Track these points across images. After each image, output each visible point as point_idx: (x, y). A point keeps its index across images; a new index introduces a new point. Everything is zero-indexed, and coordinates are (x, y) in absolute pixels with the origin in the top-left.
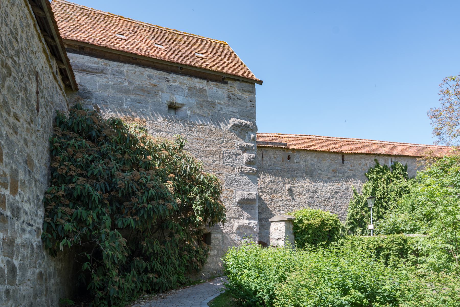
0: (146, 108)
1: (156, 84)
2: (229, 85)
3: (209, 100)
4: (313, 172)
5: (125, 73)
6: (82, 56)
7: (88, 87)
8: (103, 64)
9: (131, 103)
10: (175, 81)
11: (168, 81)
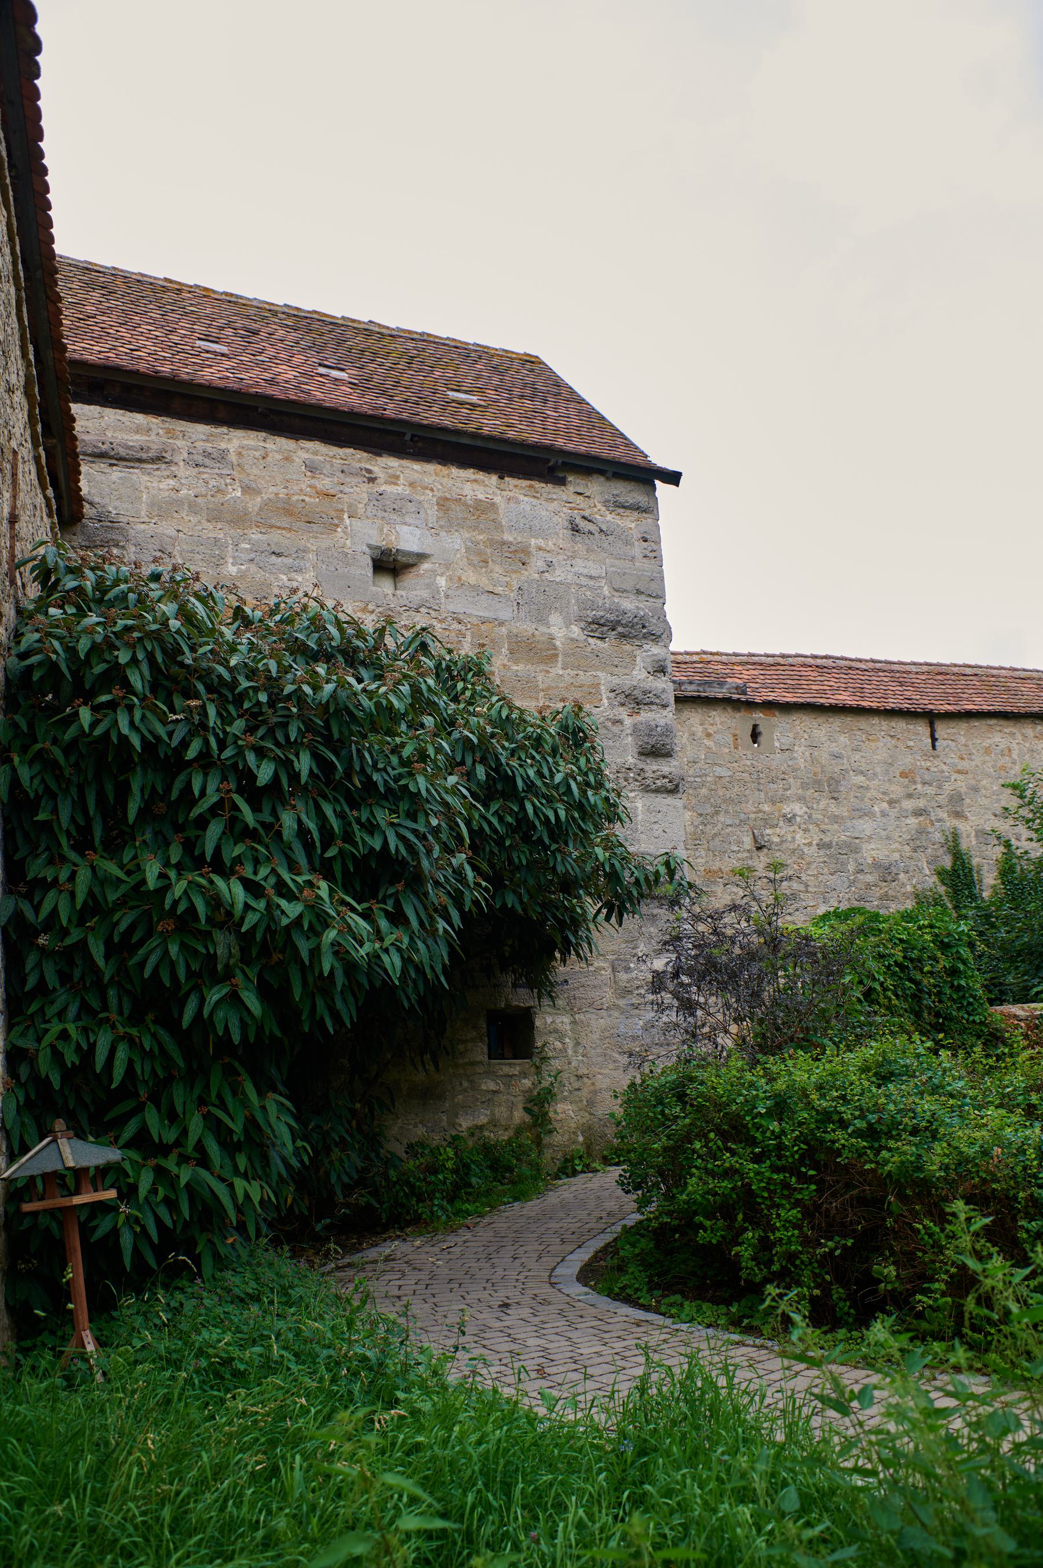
0: (299, 570)
1: (332, 492)
2: (571, 489)
3: (508, 537)
4: (838, 782)
5: (233, 457)
6: (98, 408)
7: (113, 507)
8: (161, 432)
9: (252, 556)
10: (393, 479)
11: (372, 480)
